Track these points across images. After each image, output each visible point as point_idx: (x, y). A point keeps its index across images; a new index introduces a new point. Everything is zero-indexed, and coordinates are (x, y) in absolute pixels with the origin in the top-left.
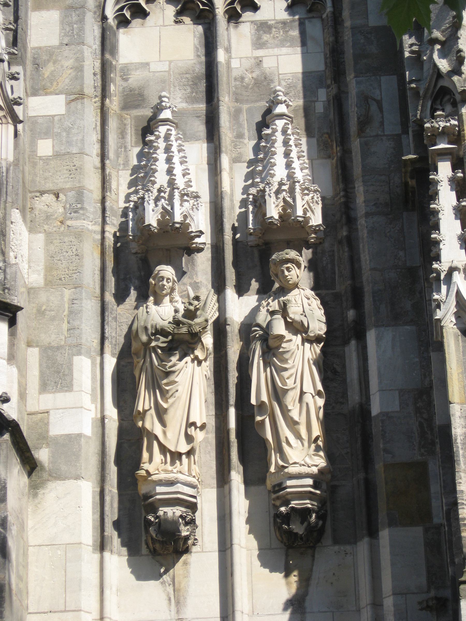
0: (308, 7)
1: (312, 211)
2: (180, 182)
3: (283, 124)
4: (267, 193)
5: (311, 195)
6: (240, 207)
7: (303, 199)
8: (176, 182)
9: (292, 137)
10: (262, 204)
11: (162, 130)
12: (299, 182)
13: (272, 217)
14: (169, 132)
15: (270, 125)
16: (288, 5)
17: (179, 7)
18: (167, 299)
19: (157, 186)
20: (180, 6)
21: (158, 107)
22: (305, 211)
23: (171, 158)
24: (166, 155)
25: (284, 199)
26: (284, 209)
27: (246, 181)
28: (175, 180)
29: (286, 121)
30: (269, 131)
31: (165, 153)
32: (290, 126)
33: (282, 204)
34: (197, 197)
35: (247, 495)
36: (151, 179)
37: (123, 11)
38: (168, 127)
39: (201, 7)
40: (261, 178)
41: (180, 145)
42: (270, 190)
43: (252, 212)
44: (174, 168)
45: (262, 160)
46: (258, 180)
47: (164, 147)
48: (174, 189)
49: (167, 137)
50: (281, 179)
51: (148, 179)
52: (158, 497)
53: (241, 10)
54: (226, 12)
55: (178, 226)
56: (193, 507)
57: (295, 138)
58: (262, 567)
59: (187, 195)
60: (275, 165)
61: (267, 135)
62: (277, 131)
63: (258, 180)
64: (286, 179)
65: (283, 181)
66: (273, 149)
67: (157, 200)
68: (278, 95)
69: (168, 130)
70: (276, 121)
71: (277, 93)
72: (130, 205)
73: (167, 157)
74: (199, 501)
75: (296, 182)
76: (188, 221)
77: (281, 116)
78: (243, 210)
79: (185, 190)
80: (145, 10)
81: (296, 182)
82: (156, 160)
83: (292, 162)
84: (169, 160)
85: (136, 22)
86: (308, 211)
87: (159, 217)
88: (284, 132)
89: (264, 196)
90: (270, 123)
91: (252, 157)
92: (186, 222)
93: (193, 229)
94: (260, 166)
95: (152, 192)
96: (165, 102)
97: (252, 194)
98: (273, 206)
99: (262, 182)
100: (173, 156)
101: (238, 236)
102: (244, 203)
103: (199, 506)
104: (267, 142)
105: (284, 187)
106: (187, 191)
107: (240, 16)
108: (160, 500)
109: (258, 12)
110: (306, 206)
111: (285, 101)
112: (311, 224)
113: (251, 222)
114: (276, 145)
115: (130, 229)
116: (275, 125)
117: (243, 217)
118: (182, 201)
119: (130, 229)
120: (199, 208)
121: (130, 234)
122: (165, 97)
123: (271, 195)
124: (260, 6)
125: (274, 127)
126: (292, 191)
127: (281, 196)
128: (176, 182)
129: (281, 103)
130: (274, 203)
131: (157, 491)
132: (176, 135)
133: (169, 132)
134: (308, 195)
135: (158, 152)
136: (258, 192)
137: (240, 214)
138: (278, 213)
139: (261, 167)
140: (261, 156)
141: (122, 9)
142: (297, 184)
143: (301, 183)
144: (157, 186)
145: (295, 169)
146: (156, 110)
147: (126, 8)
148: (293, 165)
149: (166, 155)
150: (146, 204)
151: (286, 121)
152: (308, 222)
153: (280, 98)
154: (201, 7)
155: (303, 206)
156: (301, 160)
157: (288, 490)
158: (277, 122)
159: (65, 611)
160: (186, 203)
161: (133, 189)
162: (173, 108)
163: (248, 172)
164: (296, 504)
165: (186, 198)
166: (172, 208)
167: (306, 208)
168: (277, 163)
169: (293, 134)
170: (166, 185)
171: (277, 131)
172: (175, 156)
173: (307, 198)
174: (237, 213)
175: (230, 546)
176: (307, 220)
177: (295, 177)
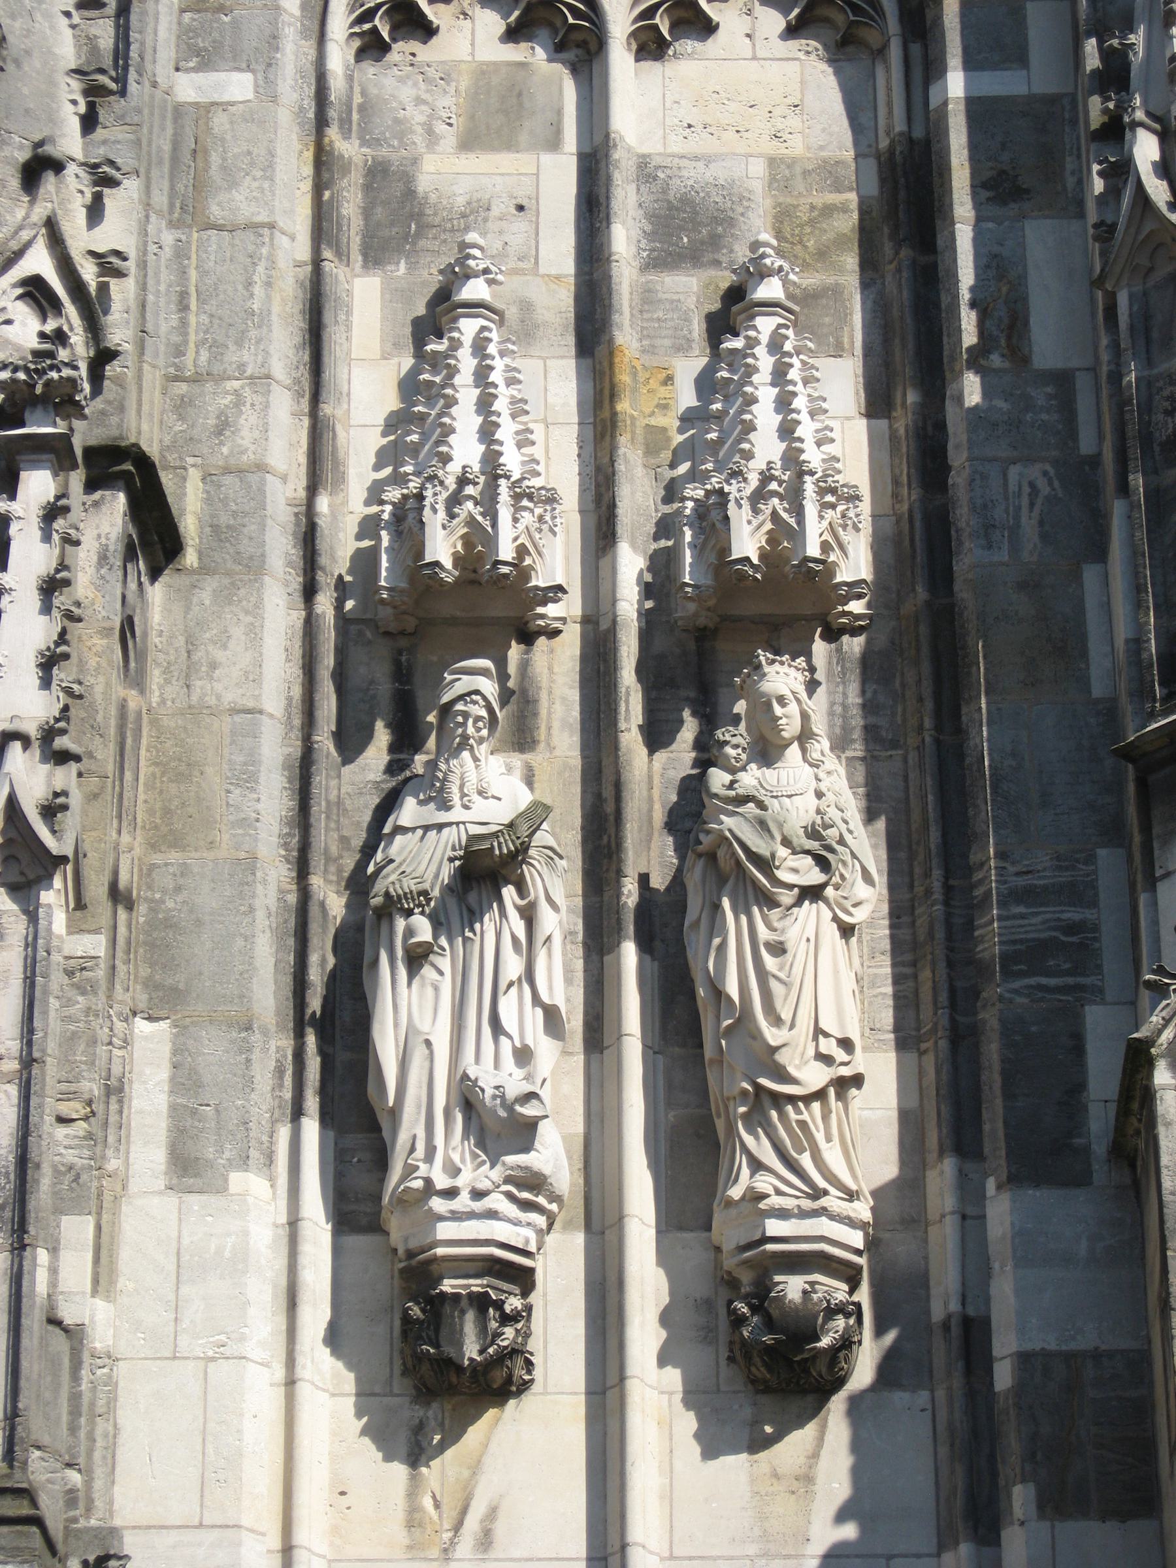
0: (557, 34)
1: (540, 554)
2: (512, 460)
3: (478, 328)
4: (427, 502)
5: (840, 508)
6: (359, 537)
7: (821, 517)
8: (502, 460)
9: (795, 361)
10: (718, 525)
11: (468, 327)
12: (812, 473)
13: (437, 564)
14: (486, 334)
15: (446, 332)
16: (788, 23)
17: (512, 18)
18: (794, 751)
19: (454, 468)
20: (516, 13)
21: (457, 269)
22: (825, 547)
23: (491, 399)
24: (777, 390)
25: (775, 515)
26: (772, 539)
27: (377, 467)
28: (802, 451)
29: (782, 321)
30: (738, 343)
31: (773, 384)
32: (790, 333)
33: (769, 526)
34: (551, 499)
35: (664, 1257)
36: (441, 449)
37: (652, 17)
38: (482, 322)
39: (571, 20)
40: (716, 462)
41: (509, 369)
42: (435, 494)
43: (693, 546)
44: (497, 425)
45: (719, 417)
46: (409, 469)
47: (770, 368)
48: (497, 477)
49: (480, 346)
50: (464, 467)
51: (430, 450)
52: (440, 1251)
53: (671, 32)
54: (634, 34)
55: (505, 570)
56: (524, 1279)
57: (507, 366)
58: (366, 1441)
59: (833, 491)
60: (453, 431)
61: (734, 351)
62: (759, 343)
63: (409, 469)
64: (779, 465)
65: (773, 471)
66: (748, 389)
67: (455, 500)
68: (763, 256)
69: (483, 329)
70: (462, 320)
71: (762, 250)
72: (383, 511)
73: (778, 396)
74: (538, 1264)
75: (501, 476)
76: (528, 561)
77: (770, 306)
78: (366, 543)
79: (830, 479)
80: (708, 20)
81: (501, 476)
82: (752, 400)
83: (497, 425)
84: (485, 405)
85: (688, 45)
86: (833, 550)
87: (459, 548)
88: (480, 346)
89: (421, 509)
90: (742, 323)
91: (694, 402)
92: (525, 563)
93: (539, 580)
94: (415, 432)
95: (442, 483)
96: (475, 258)
97: (692, 499)
98: (747, 529)
99: (417, 473)
100: (496, 396)
101: (349, 604)
102: (369, 527)
103: (539, 1277)
104: (732, 368)
105: (470, 490)
106: (528, 487)
107: (668, 45)
108: (775, 1255)
109: (435, 40)
110: (827, 536)
111: (486, 271)
112: (533, 583)
113: (384, 574)
114: (457, 380)
115: (688, 569)
116: (755, 328)
117: (365, 562)
118: (517, 508)
119: (688, 569)
120: (860, 526)
121: (687, 580)
122: (474, 246)
123: (742, 502)
124: (438, 27)
125: (752, 333)
126: (489, 503)
127: (766, 509)
128: (502, 460)
129: (477, 276)
130: (749, 522)
131: (769, 1233)
132: (499, 343)
133: (486, 334)
134: (833, 506)
135: (756, 378)
136: (708, 493)
137: (358, 555)
138: (760, 548)
139: (417, 436)
140: (717, 406)
141: (650, 12)
142: (807, 478)
143: (817, 476)
144: (454, 468)
145: (501, 444)
146: (452, 277)
147: (380, 13)
148: (498, 435)
149: (777, 390)
150: (427, 512)
151: (782, 321)
152: (528, 578)
153: (768, 261)
154: (571, 20)
155: (516, 539)
156: (819, 421)
157: (770, 1247)
158: (464, 323)
159: (201, 1525)
160: (524, 514)
161: (388, 470)
162: (788, 273)
163: (384, 446)
164: (453, 1286)
165: (525, 502)
166: (494, 525)
167: (523, 545)
168: (758, 423)
169: (502, 354)
170: (476, 467)
171: (759, 343)
172: (500, 396)
173: (829, 514)
174: (350, 552)
175: (616, 1380)
176: (830, 570)
177: (804, 462)
